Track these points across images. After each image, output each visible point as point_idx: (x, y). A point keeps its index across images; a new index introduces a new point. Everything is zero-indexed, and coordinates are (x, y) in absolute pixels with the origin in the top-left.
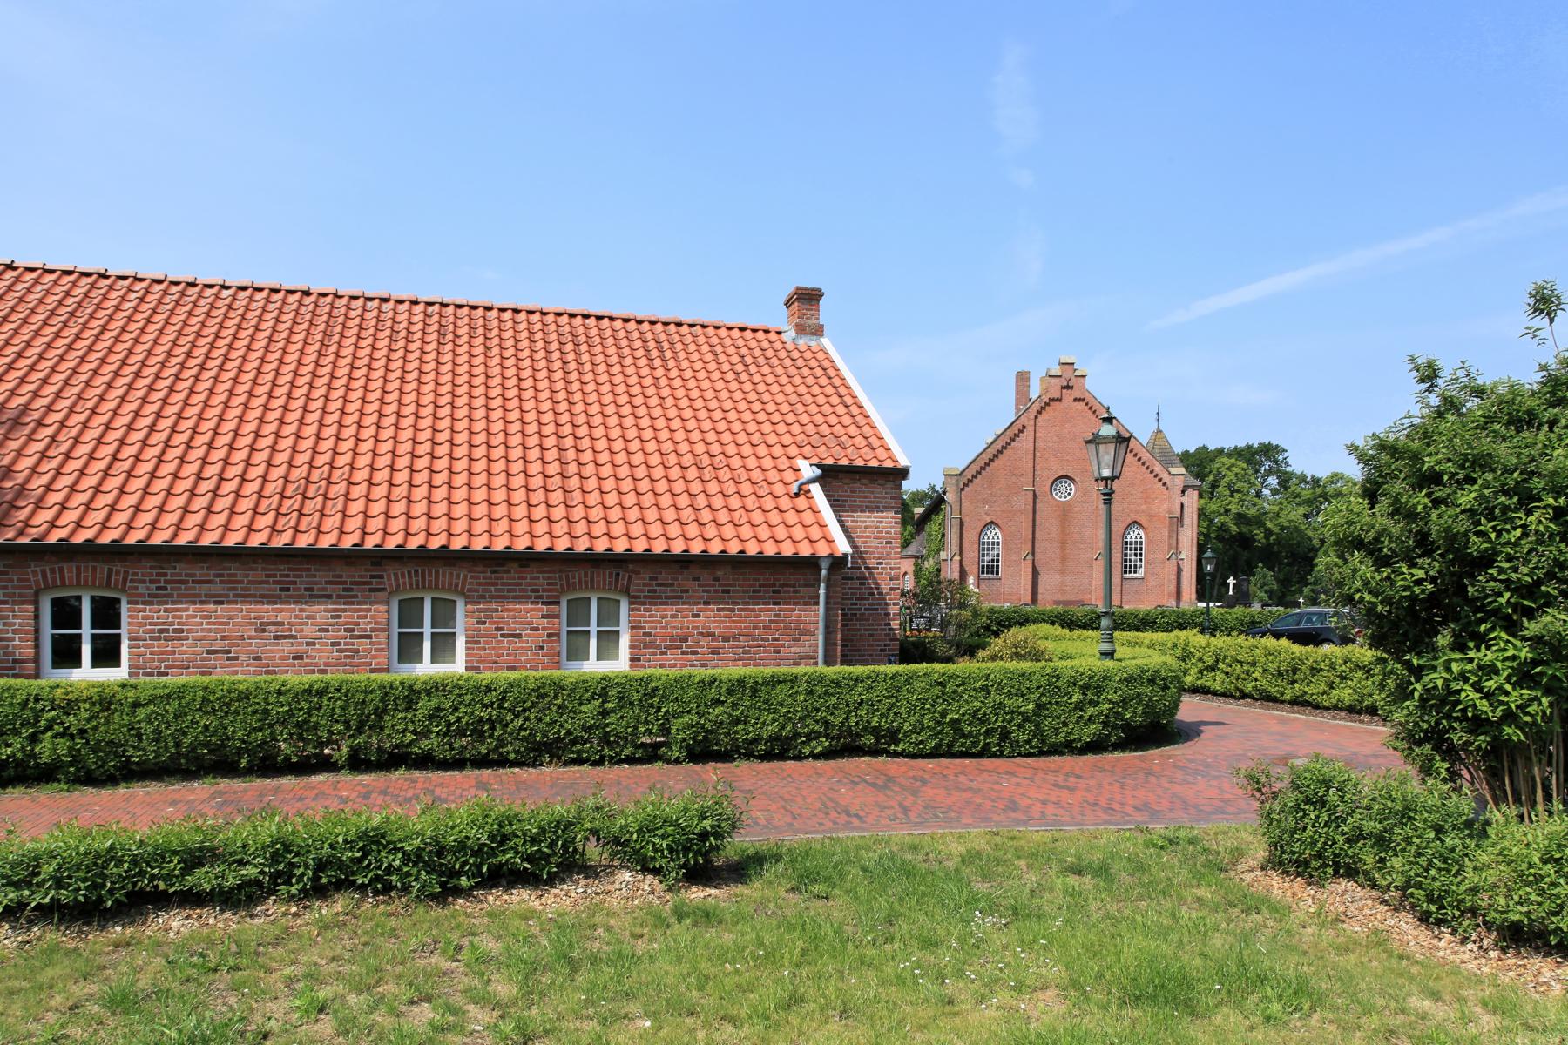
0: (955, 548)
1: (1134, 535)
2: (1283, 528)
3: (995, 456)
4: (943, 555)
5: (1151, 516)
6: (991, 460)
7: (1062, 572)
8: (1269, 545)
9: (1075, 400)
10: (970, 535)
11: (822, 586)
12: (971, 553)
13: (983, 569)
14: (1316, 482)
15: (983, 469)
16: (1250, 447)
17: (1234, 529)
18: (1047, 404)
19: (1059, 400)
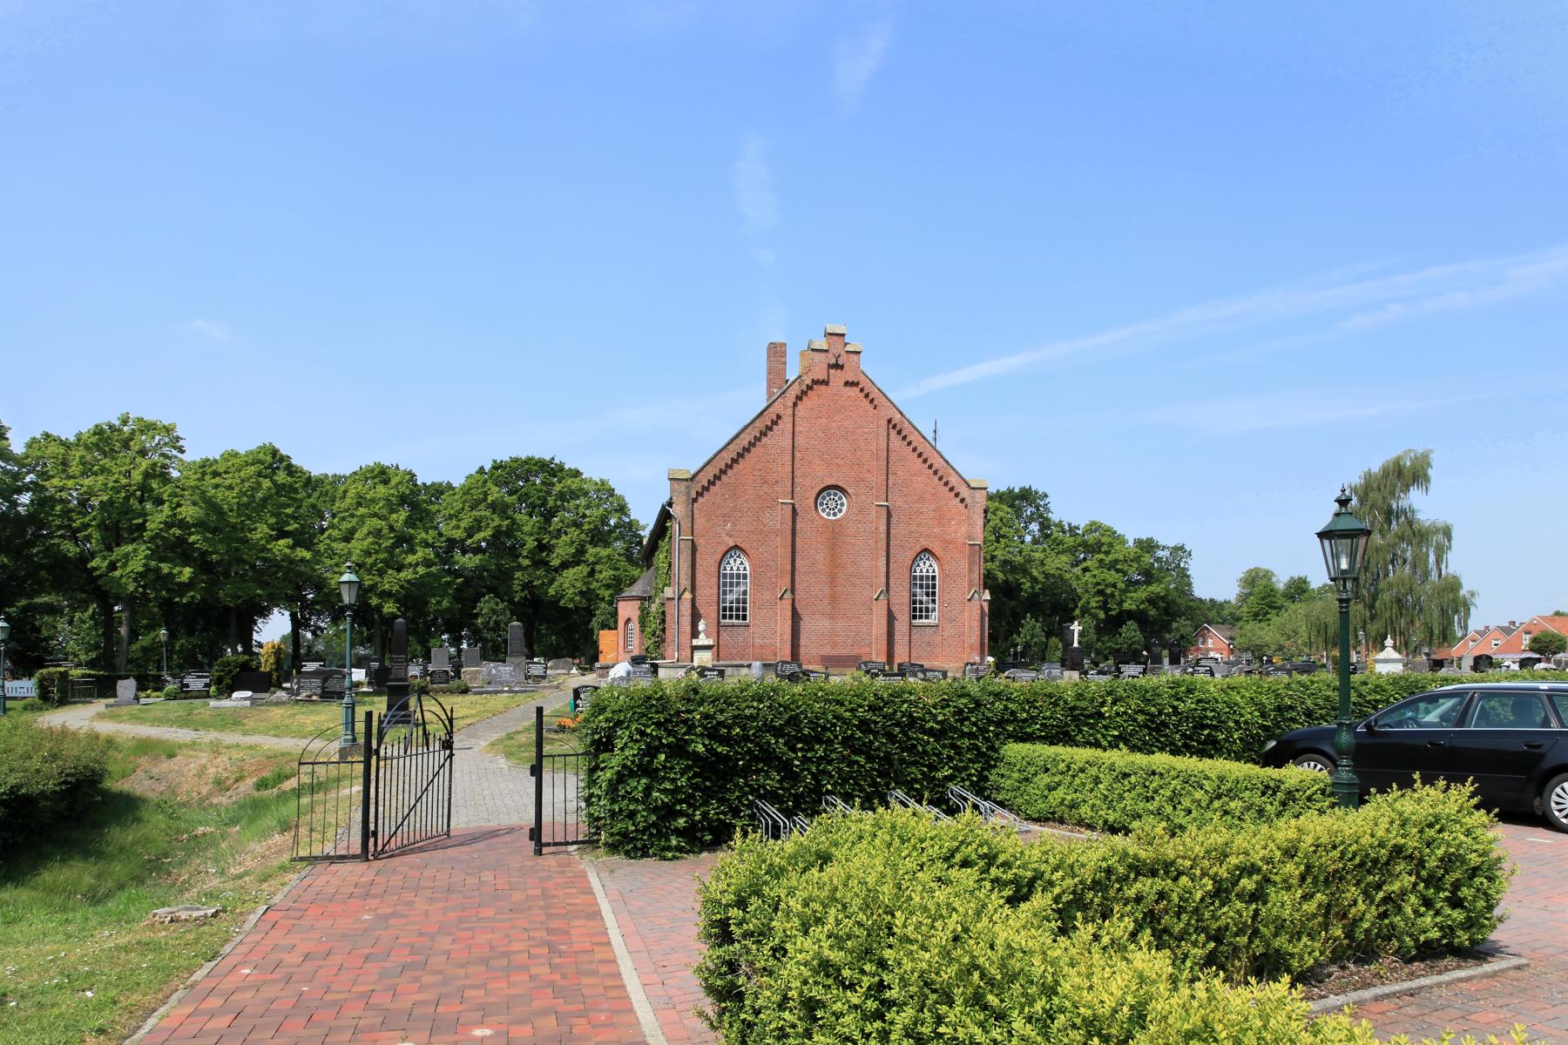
0: (686, 582)
1: (926, 567)
2: (1047, 576)
3: (740, 455)
4: (669, 592)
5: (947, 543)
6: (734, 461)
7: (832, 617)
8: (1035, 595)
9: (847, 383)
10: (706, 563)
11: (38, 600)
12: (707, 592)
13: (724, 612)
14: (1073, 530)
15: (723, 472)
16: (1011, 491)
17: (1001, 576)
18: (810, 388)
19: (825, 383)
